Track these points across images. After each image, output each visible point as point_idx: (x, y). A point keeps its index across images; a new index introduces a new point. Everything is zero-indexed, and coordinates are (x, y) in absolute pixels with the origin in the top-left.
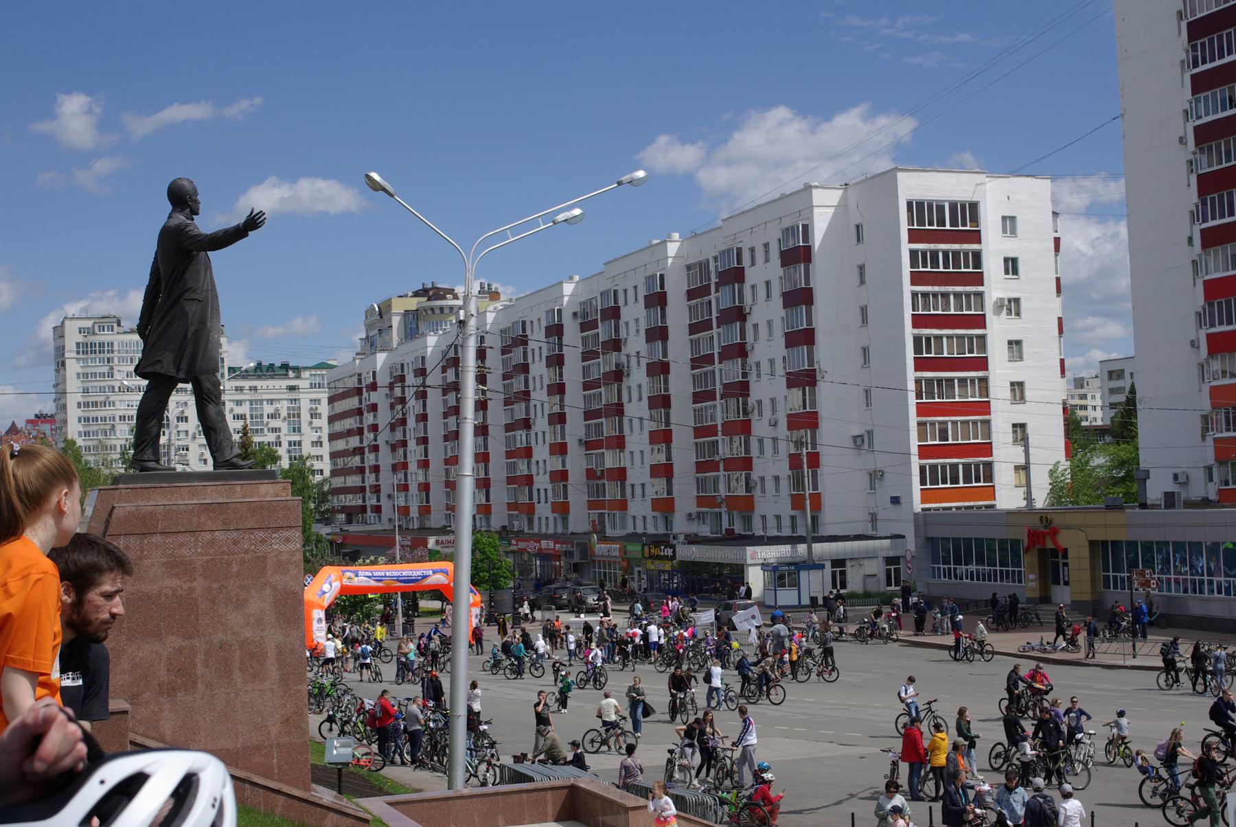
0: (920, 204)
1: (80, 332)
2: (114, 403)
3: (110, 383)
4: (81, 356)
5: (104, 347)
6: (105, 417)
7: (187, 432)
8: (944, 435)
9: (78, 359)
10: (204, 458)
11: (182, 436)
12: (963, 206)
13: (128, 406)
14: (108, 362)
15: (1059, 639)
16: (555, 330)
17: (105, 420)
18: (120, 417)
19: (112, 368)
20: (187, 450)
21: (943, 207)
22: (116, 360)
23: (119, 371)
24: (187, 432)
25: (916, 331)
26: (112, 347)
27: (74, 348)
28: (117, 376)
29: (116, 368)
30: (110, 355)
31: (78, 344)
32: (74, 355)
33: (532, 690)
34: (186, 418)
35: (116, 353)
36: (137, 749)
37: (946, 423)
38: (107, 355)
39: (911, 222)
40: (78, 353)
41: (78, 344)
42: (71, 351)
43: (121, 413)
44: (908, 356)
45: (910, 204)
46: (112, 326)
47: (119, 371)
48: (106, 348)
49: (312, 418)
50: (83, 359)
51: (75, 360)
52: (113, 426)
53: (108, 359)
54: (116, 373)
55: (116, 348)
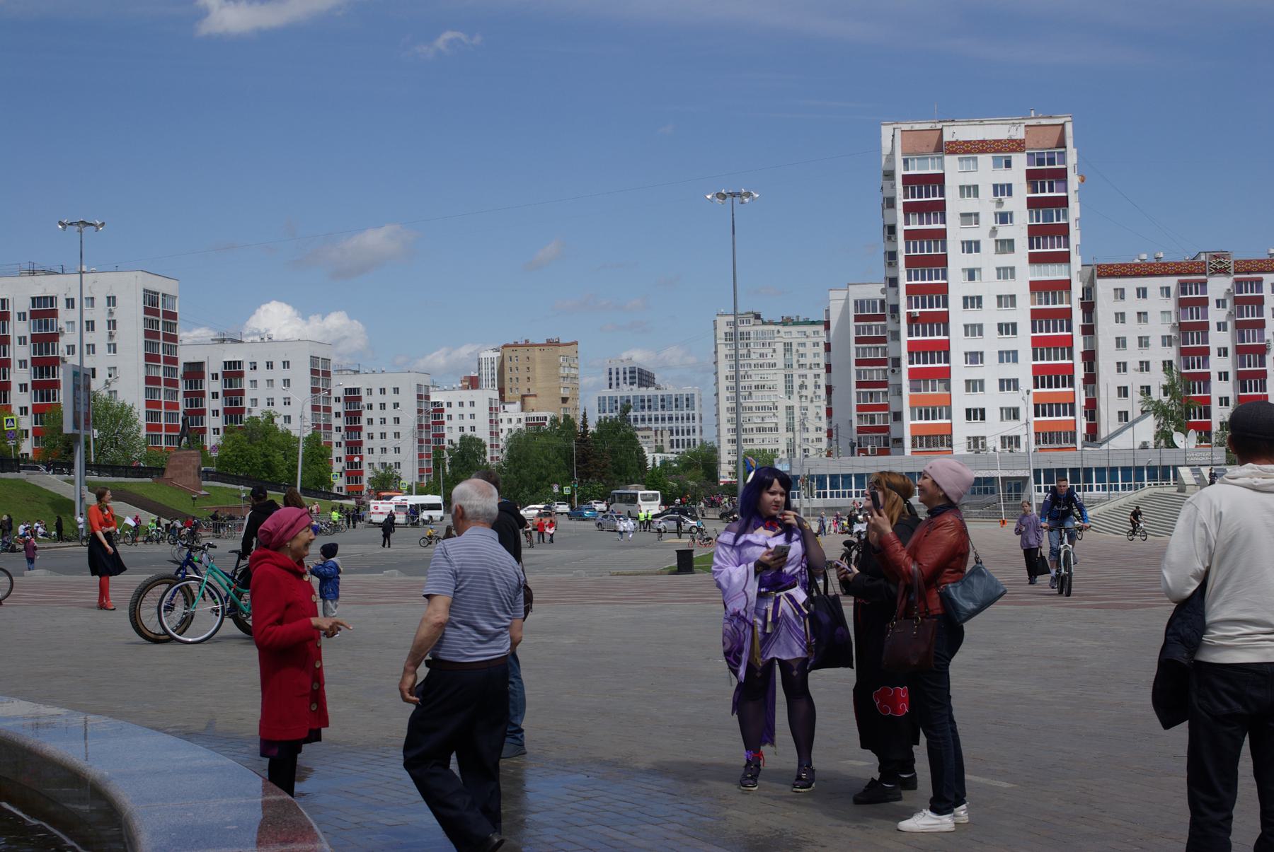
0: (862, 302)
1: (728, 325)
2: (751, 376)
3: (748, 362)
4: (728, 342)
5: (744, 335)
6: (758, 386)
7: (806, 396)
8: (873, 421)
9: (726, 345)
10: (819, 415)
11: (803, 399)
12: (868, 302)
13: (761, 378)
14: (747, 346)
15: (793, 556)
16: (618, 384)
17: (745, 389)
18: (755, 386)
19: (749, 351)
20: (807, 410)
21: (876, 303)
22: (752, 345)
23: (754, 353)
24: (806, 396)
25: (857, 368)
26: (749, 335)
27: (723, 336)
28: (753, 356)
29: (752, 351)
30: (748, 341)
31: (726, 334)
32: (723, 341)
33: (415, 596)
34: (806, 386)
35: (752, 340)
36: (416, 685)
37: (874, 415)
38: (746, 341)
39: (856, 311)
40: (726, 340)
41: (726, 334)
42: (720, 339)
43: (756, 383)
44: (852, 381)
45: (856, 302)
46: (749, 320)
47: (754, 353)
48: (745, 336)
49: (816, 388)
50: (730, 344)
51: (724, 345)
52: (750, 393)
53: (747, 344)
54: (752, 354)
55: (752, 336)
